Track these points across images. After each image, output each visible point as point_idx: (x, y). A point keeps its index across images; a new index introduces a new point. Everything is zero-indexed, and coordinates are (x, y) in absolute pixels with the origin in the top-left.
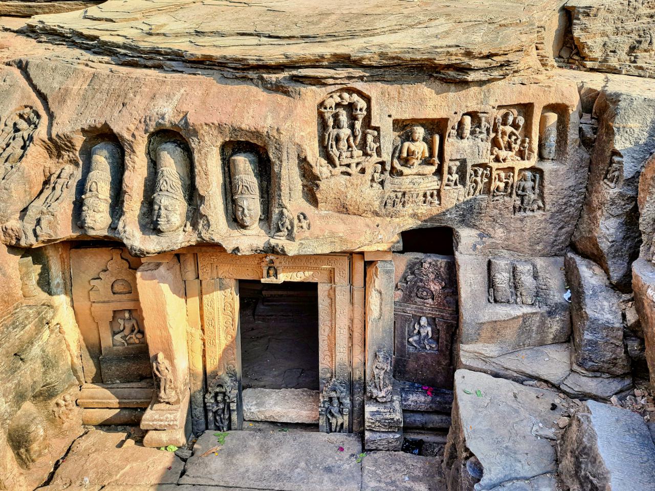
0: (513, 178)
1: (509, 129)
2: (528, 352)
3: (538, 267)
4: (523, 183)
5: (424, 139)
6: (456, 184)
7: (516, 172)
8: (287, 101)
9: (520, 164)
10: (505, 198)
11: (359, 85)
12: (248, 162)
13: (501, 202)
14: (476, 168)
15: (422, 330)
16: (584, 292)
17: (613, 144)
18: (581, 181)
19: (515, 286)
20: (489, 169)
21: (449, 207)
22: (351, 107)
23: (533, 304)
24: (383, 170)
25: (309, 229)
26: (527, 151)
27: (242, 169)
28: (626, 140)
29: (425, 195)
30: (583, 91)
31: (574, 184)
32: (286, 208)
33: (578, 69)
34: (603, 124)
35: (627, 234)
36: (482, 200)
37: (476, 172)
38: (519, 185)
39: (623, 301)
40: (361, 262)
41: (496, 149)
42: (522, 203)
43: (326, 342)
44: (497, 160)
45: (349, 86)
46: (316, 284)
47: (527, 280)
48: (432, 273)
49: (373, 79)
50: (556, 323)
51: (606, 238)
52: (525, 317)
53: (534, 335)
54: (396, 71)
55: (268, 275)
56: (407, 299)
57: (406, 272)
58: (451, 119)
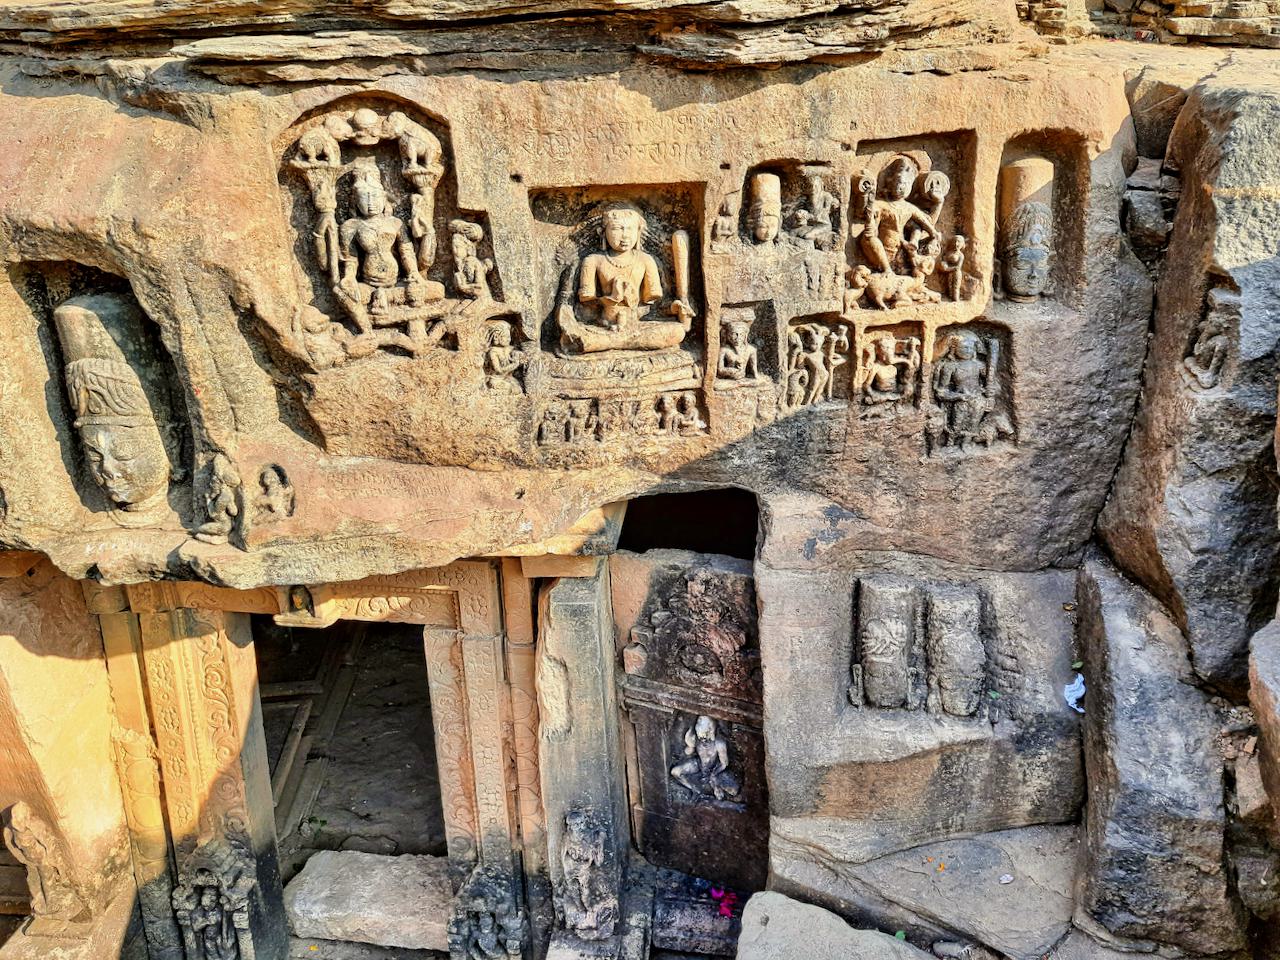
0: (921, 353)
1: (903, 210)
2: (958, 850)
3: (998, 601)
4: (951, 367)
5: (649, 246)
6: (749, 373)
7: (930, 336)
8: (180, 138)
9: (938, 313)
10: (900, 408)
11: (404, 85)
12: (97, 322)
13: (886, 421)
14: (807, 327)
15: (702, 751)
16: (1112, 699)
17: (1212, 248)
18: (1125, 357)
19: (924, 657)
20: (844, 328)
21: (735, 436)
22: (390, 150)
23: (972, 715)
24: (518, 340)
25: (291, 513)
26: (959, 274)
27: (83, 342)
28: (1252, 236)
29: (660, 406)
30: (1139, 94)
31: (1103, 367)
32: (224, 453)
33: (1156, 38)
34: (1190, 190)
35: (1247, 528)
36: (832, 416)
37: (807, 337)
38: (942, 372)
39: (1231, 734)
40: (521, 586)
41: (865, 270)
42: (951, 420)
43: (456, 775)
44: (869, 300)
45: (371, 86)
46: (418, 629)
47: (960, 646)
48: (713, 607)
49: (442, 64)
50: (1039, 771)
51: (1181, 537)
52: (948, 754)
53: (975, 802)
54: (514, 40)
55: (293, 608)
56: (658, 669)
57: (650, 601)
58: (712, 184)
